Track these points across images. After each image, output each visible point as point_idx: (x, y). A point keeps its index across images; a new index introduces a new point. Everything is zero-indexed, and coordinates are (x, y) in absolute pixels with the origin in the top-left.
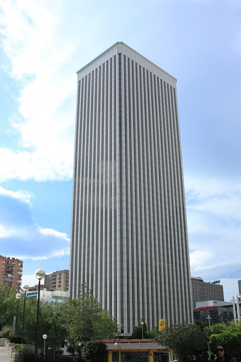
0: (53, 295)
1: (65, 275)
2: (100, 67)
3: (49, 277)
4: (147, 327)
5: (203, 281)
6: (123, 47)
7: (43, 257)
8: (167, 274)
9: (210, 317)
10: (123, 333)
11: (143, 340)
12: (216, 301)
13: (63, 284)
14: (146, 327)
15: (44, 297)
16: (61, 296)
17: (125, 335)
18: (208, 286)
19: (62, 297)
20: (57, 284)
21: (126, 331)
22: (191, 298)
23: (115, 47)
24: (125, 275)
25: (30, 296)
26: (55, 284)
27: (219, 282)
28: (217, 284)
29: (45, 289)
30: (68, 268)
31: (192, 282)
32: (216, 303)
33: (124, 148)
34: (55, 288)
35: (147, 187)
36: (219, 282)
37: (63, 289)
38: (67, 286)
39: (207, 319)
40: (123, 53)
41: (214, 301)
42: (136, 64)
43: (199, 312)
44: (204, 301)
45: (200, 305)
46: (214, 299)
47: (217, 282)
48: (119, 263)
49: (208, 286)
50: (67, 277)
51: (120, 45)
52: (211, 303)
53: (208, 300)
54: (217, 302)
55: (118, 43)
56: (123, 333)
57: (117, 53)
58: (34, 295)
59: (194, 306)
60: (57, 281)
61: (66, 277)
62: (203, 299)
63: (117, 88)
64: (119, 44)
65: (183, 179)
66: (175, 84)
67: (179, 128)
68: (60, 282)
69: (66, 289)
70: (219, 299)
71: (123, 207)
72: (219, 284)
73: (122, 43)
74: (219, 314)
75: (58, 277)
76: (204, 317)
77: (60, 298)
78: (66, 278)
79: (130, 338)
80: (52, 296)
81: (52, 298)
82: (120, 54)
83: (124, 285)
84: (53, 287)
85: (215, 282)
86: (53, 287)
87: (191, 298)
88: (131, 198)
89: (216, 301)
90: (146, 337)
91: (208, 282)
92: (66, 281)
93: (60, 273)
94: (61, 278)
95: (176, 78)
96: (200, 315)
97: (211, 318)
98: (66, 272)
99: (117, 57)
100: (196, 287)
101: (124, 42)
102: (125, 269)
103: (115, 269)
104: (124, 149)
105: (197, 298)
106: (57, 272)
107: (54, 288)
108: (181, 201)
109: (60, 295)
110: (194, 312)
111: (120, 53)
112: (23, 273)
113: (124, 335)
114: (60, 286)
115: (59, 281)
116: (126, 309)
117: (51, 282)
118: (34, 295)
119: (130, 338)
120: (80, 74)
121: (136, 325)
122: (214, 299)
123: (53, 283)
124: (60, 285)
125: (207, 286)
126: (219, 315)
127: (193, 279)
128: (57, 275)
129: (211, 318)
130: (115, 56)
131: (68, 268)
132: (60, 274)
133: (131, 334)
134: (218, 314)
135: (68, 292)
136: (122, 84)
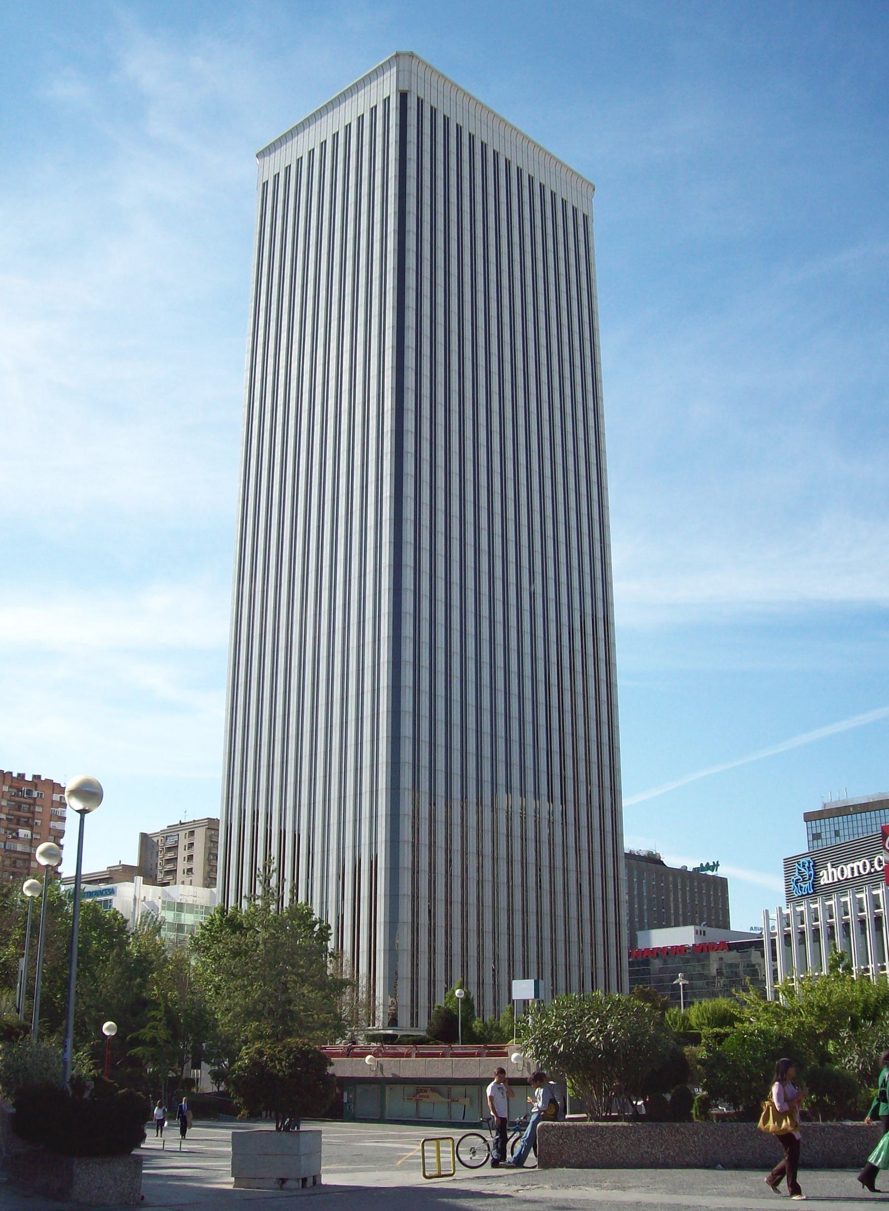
0: (168, 900)
1: (208, 834)
3: (155, 840)
4: (476, 1007)
5: (662, 863)
8: (546, 885)
9: (684, 978)
10: (396, 1026)
11: (458, 1047)
13: (199, 863)
14: (473, 1007)
15: (135, 904)
16: (191, 902)
17: (399, 1033)
19: (197, 906)
20: (182, 865)
21: (404, 1018)
22: (624, 919)
26: (176, 854)
27: (715, 866)
28: (709, 873)
30: (216, 812)
31: (628, 866)
32: (704, 934)
33: (409, 455)
34: (175, 878)
35: (485, 612)
36: (715, 866)
37: (201, 880)
40: (414, 89)
41: (698, 928)
47: (708, 867)
52: (683, 936)
56: (396, 1026)
58: (103, 898)
59: (633, 940)
60: (182, 854)
65: (615, 660)
66: (589, 200)
67: (595, 316)
68: (190, 858)
69: (209, 882)
70: (713, 923)
72: (714, 873)
76: (661, 980)
77: (192, 908)
78: (209, 844)
79: (418, 1041)
80: (164, 902)
81: (163, 908)
83: (405, 432)
84: (168, 873)
85: (702, 868)
86: (168, 873)
87: (624, 919)
88: (431, 512)
90: (471, 1038)
91: (678, 866)
93: (190, 829)
94: (192, 844)
95: (594, 183)
96: (649, 974)
98: (211, 824)
100: (640, 882)
103: (374, 666)
105: (641, 916)
106: (181, 823)
107: (170, 877)
108: (603, 676)
110: (631, 964)
111: (407, 88)
113: (396, 1033)
114: (190, 870)
115: (186, 854)
116: (405, 947)
117: (156, 859)
118: (103, 898)
119: (418, 1041)
120: (267, 159)
122: (697, 921)
123: (169, 861)
127: (631, 856)
128: (182, 834)
129: (687, 982)
131: (216, 812)
132: (192, 833)
133: (422, 1031)
135: (214, 890)
136: (410, 194)
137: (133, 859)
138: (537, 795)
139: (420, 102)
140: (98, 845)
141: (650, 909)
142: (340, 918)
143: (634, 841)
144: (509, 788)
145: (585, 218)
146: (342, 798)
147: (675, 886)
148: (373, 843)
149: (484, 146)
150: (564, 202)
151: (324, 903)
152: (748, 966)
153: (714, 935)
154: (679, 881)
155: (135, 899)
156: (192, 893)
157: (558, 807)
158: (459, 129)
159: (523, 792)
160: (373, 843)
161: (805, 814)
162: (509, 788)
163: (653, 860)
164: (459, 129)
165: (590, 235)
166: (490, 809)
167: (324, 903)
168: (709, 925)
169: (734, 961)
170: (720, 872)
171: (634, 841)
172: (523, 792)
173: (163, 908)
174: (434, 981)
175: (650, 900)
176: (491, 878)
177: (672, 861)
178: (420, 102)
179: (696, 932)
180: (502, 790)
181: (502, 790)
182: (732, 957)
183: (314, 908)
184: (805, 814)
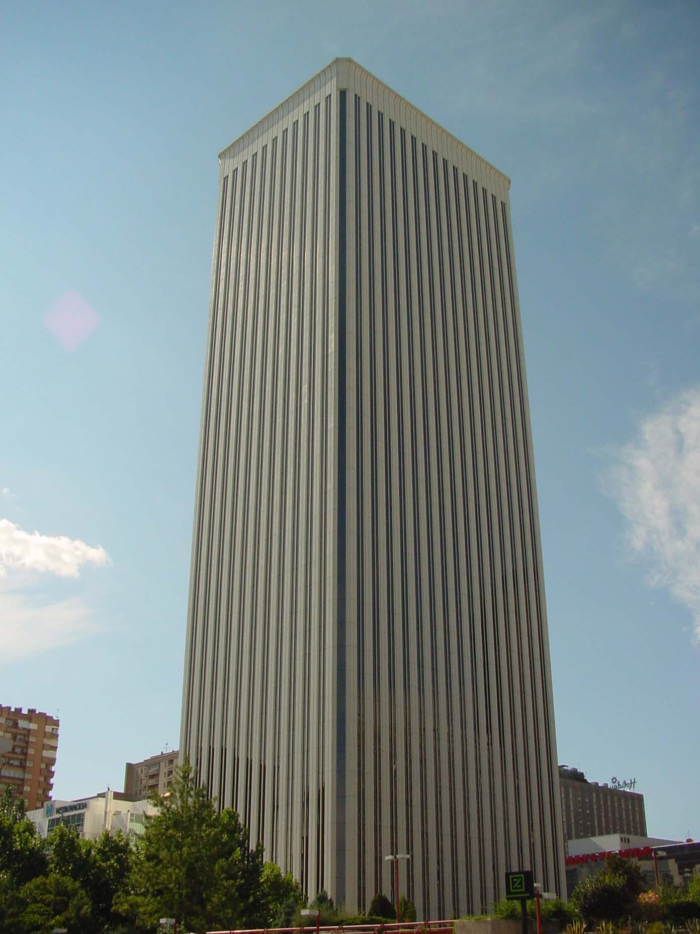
12: (627, 836)
18: (616, 799)
23: (328, 76)
25: (66, 814)
27: (633, 783)
36: (633, 783)
41: (623, 836)
45: (579, 847)
49: (616, 799)
52: (611, 843)
53: (593, 835)
54: (632, 838)
55: (337, 61)
58: (77, 812)
59: (565, 847)
62: (588, 831)
72: (631, 791)
73: (349, 60)
75: (164, 770)
80: (132, 815)
81: (132, 821)
89: (627, 836)
105: (569, 830)
111: (345, 87)
112: (59, 755)
118: (77, 812)
120: (227, 160)
125: (619, 800)
126: (159, 814)
139: (357, 99)
146: (267, 602)
148: (320, 772)
149: (465, 177)
150: (445, 162)
151: (289, 855)
153: (636, 842)
154: (601, 796)
155: (106, 812)
158: (380, 115)
160: (320, 772)
163: (577, 777)
164: (380, 115)
167: (289, 855)
168: (629, 833)
170: (637, 790)
173: (132, 821)
174: (380, 827)
177: (590, 779)
178: (357, 99)
179: (621, 839)
183: (279, 865)
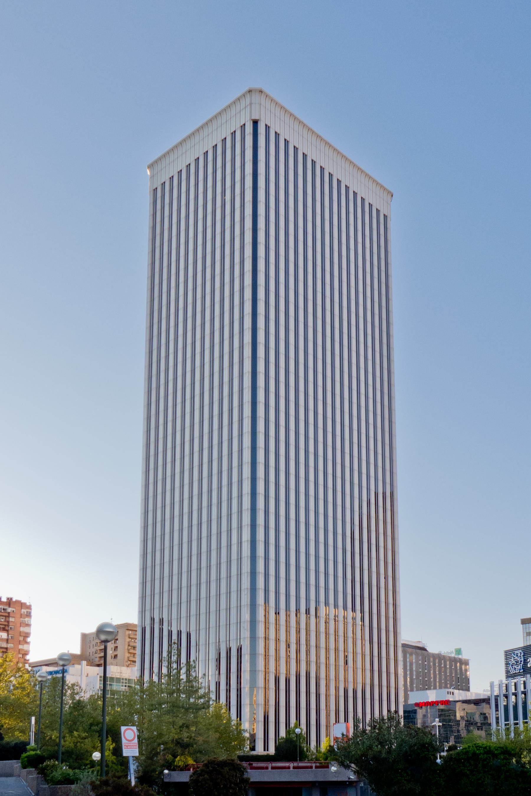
2: (224, 140)
5: (425, 650)
6: (263, 102)
7: (73, 598)
9: (440, 722)
16: (119, 677)
19: (123, 679)
24: (260, 650)
29: (84, 663)
32: (453, 694)
38: (132, 655)
39: (433, 725)
40: (263, 119)
42: (313, 162)
43: (415, 712)
44: (427, 689)
45: (415, 697)
46: (449, 686)
48: (248, 517)
50: (132, 638)
51: (256, 97)
57: (248, 118)
61: (129, 638)
62: (426, 686)
63: (260, 599)
64: (253, 93)
71: (257, 603)
74: (458, 718)
82: (255, 123)
92: (129, 645)
94: (117, 647)
95: (392, 191)
97: (441, 724)
99: (249, 129)
101: (264, 89)
102: (260, 673)
104: (261, 406)
109: (117, 674)
110: (405, 712)
111: (257, 118)
114: (116, 656)
121: (283, 733)
122: (449, 686)
124: (117, 647)
127: (404, 646)
129: (441, 724)
130: (224, 140)
134: (455, 716)
137: (76, 650)
138: (345, 608)
140: (51, 639)
141: (417, 677)
142: (218, 684)
143: (408, 634)
144: (327, 604)
145: (385, 217)
147: (434, 664)
152: (481, 714)
156: (119, 671)
157: (358, 615)
159: (336, 606)
161: (468, 660)
162: (327, 604)
165: (389, 266)
166: (314, 617)
169: (473, 711)
171: (408, 634)
172: (336, 606)
175: (418, 673)
176: (352, 681)
177: (432, 649)
180: (322, 605)
181: (322, 605)
182: (471, 708)
184: (468, 660)
